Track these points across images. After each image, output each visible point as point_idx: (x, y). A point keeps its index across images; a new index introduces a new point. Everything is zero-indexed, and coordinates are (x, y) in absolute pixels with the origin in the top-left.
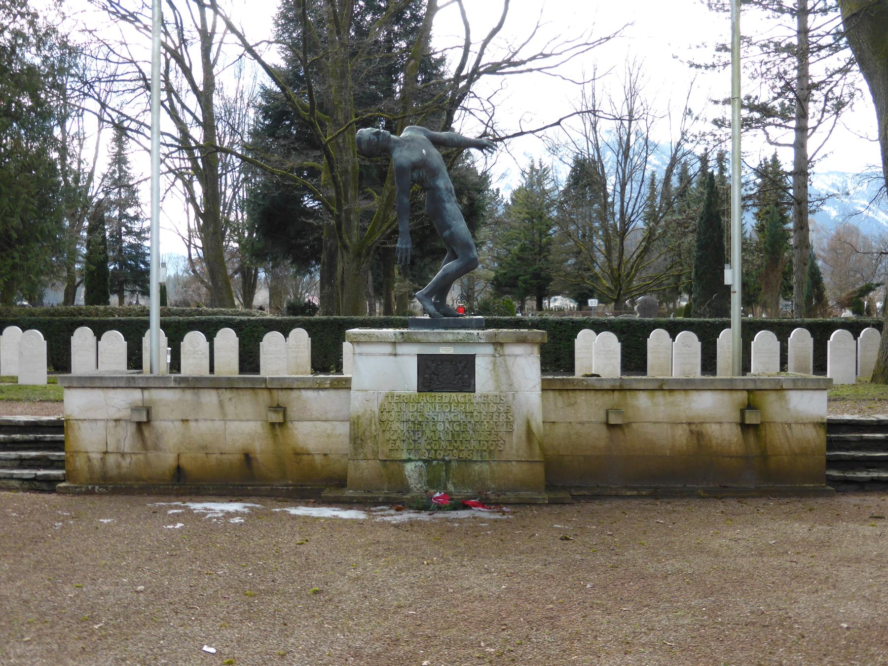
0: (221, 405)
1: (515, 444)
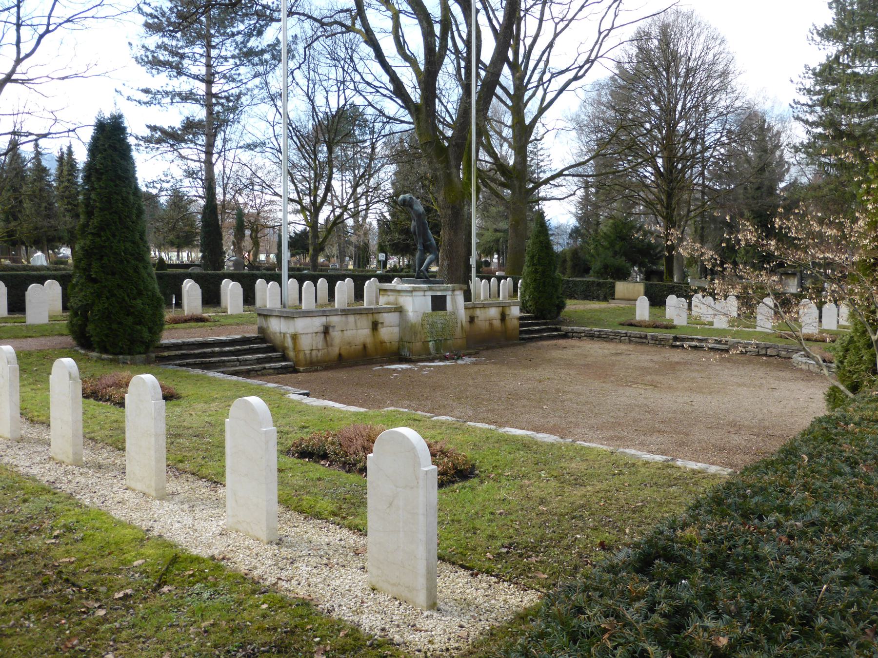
0: (355, 321)
1: (458, 332)
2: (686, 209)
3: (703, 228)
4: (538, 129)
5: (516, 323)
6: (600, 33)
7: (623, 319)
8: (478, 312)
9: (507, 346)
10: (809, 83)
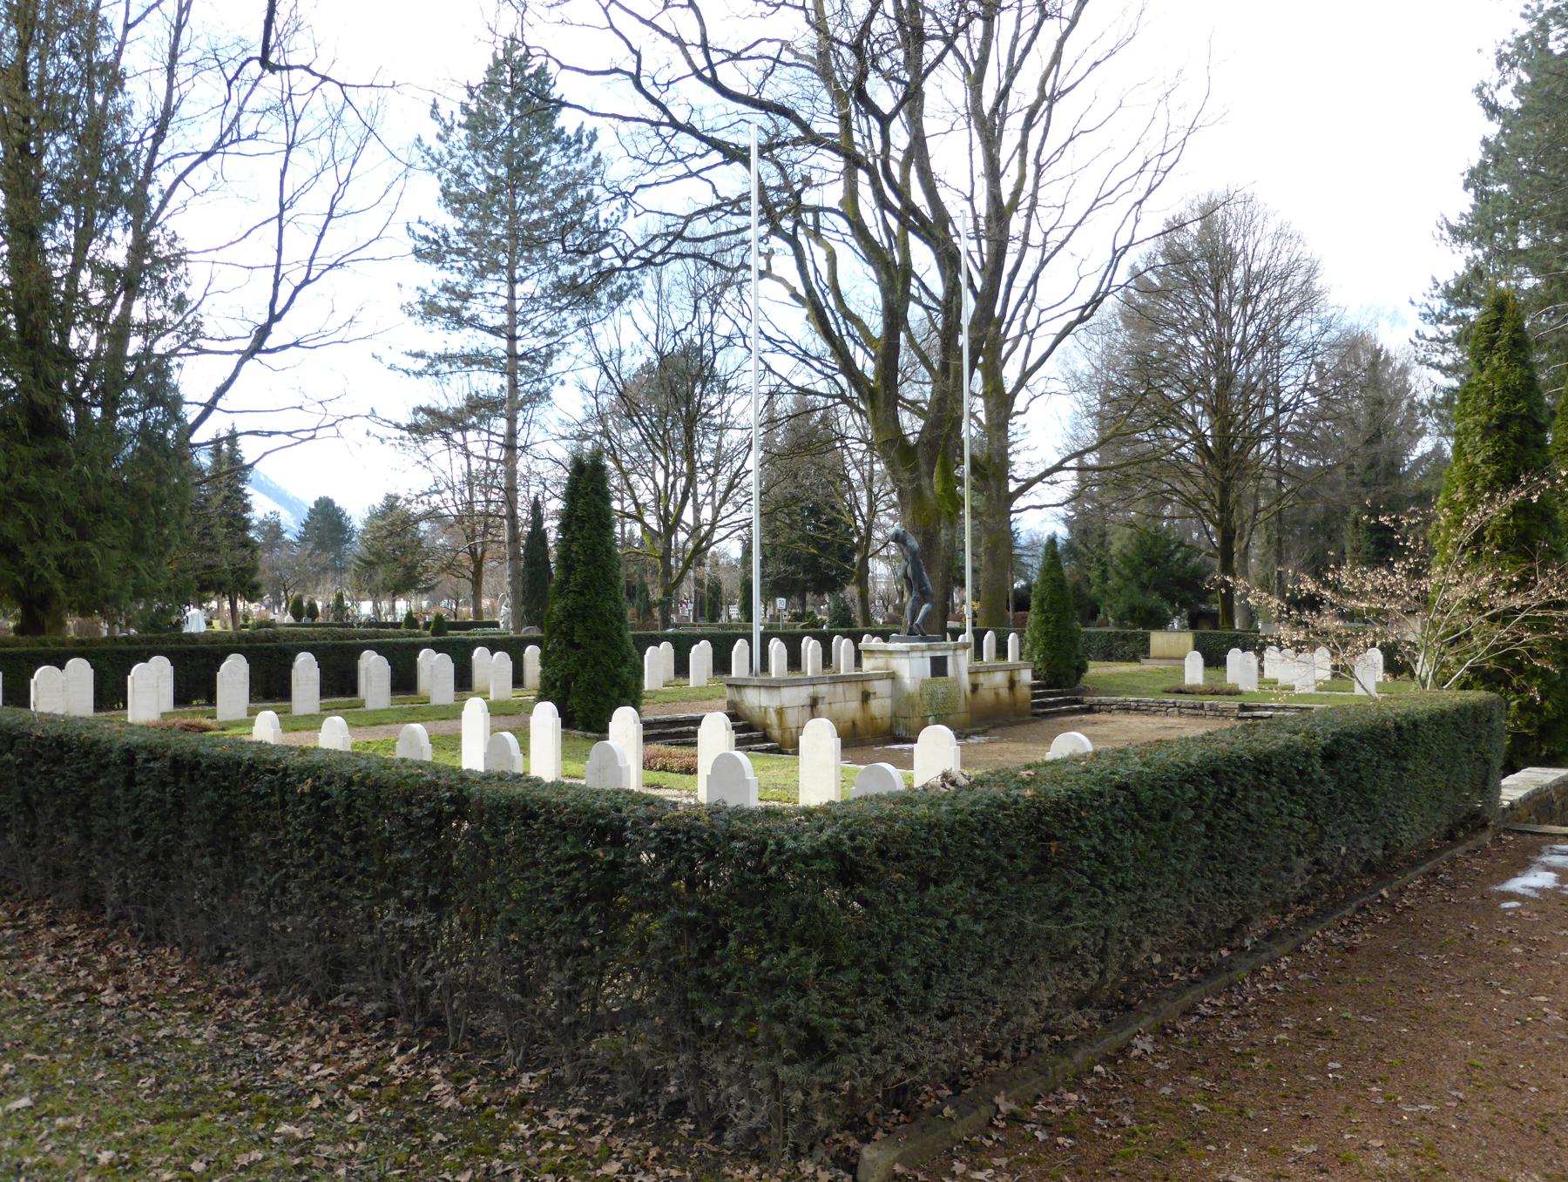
2: (1251, 508)
3: (1279, 540)
4: (1020, 403)
5: (1027, 692)
6: (1115, 252)
7: (1166, 685)
8: (982, 678)
9: (1019, 723)
10: (1439, 305)
